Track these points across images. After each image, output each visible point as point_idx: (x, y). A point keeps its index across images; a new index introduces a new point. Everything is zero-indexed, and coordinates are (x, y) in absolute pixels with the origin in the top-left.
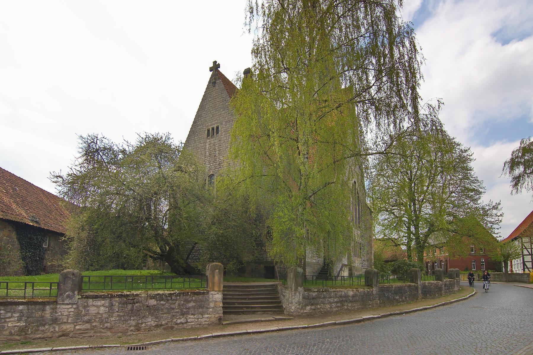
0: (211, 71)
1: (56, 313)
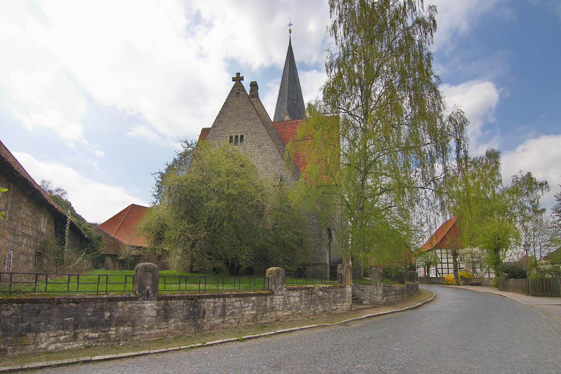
0: (233, 81)
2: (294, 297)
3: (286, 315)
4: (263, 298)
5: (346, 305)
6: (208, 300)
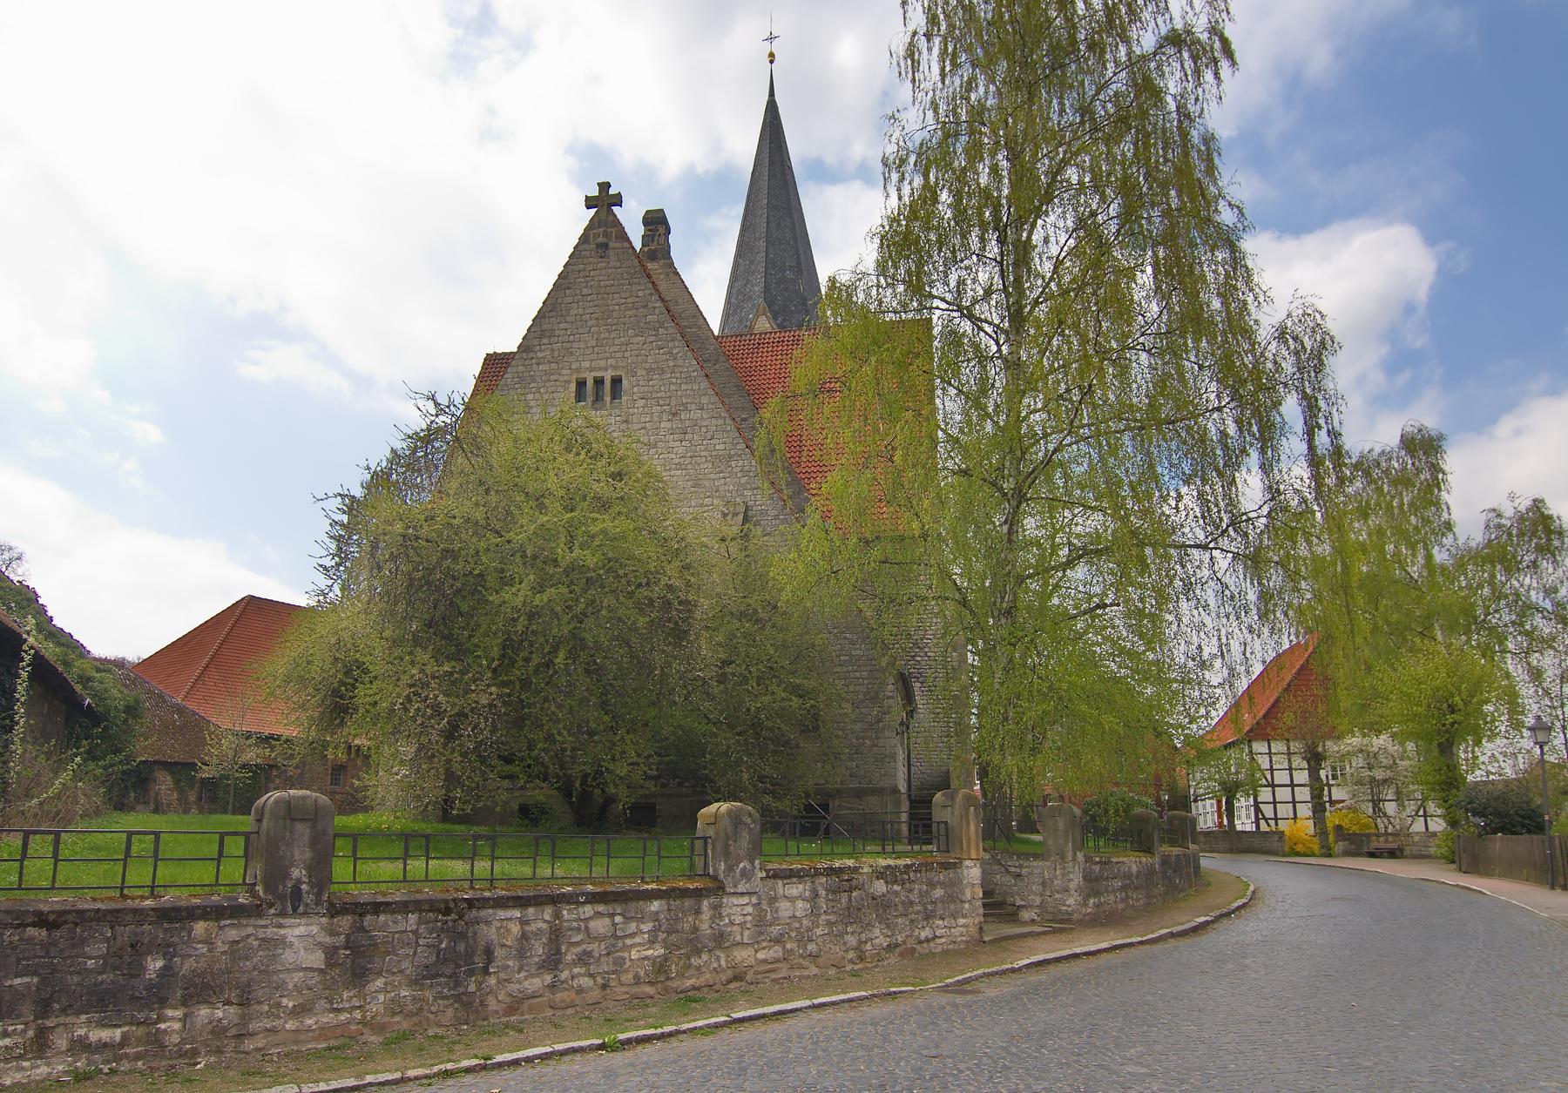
1: (721, 917)
2: (792, 900)
3: (764, 961)
4: (688, 903)
5: (964, 925)
6: (502, 914)
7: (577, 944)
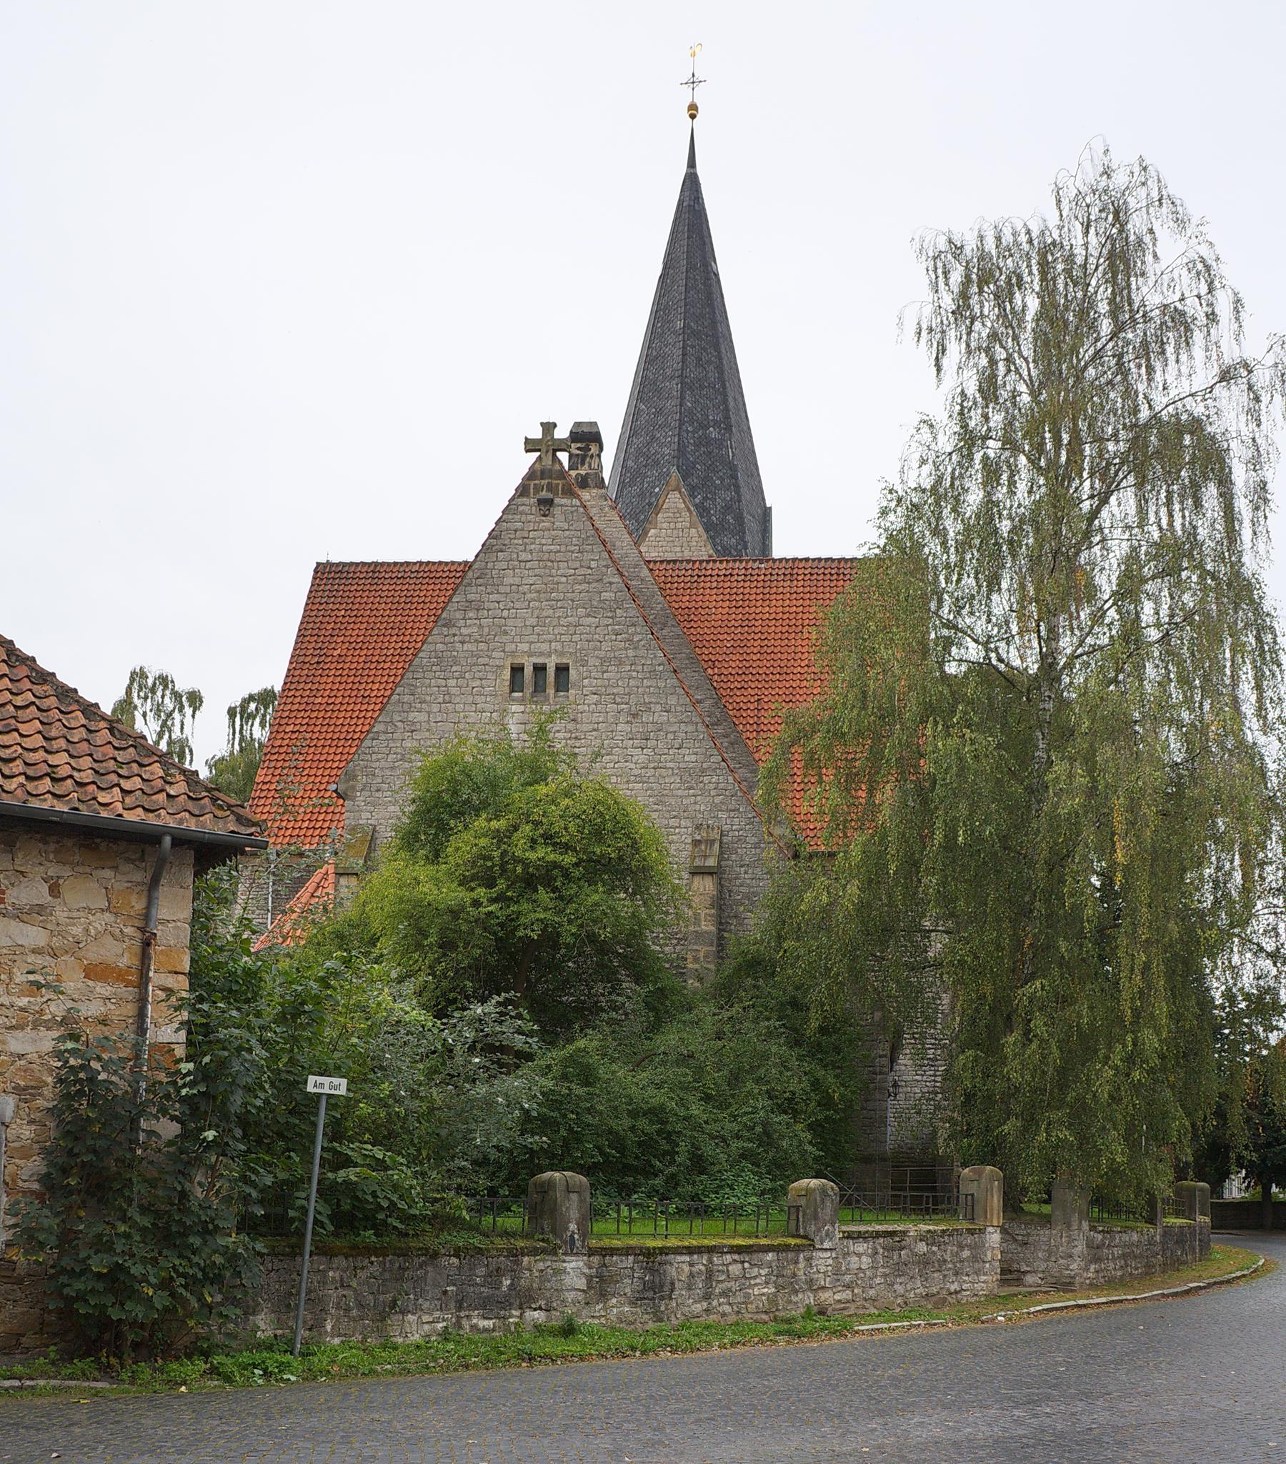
1: (811, 1266)
2: (859, 1255)
3: (839, 1301)
4: (791, 1255)
5: (987, 1281)
6: (679, 1258)
7: (722, 1282)
